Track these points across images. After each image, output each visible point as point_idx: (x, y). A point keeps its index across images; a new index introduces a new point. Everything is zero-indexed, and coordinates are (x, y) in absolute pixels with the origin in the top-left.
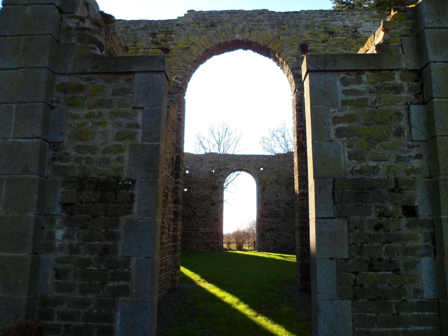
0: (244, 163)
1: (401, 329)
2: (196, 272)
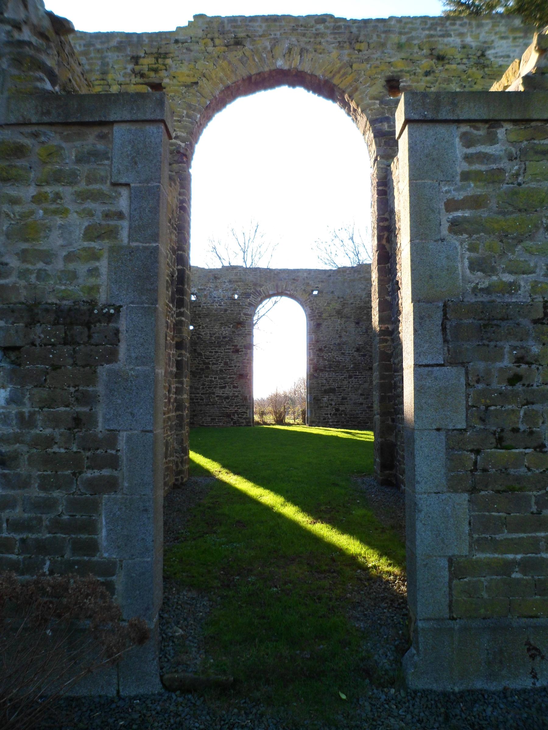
0: (287, 282)
1: (543, 534)
2: (214, 459)
